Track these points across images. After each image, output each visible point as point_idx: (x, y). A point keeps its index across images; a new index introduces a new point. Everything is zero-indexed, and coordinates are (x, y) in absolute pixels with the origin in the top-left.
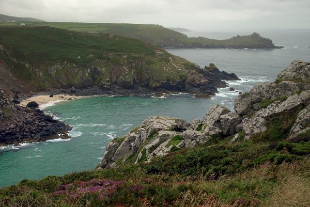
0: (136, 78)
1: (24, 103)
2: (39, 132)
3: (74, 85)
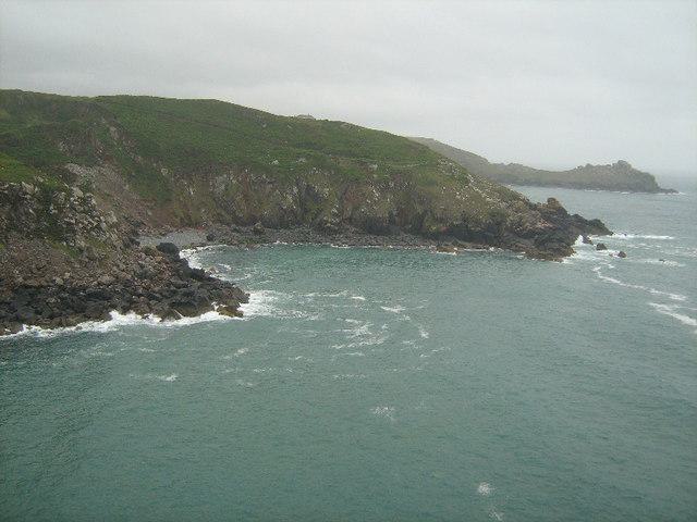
0: (394, 213)
1: (149, 241)
2: (167, 298)
3: (262, 218)
